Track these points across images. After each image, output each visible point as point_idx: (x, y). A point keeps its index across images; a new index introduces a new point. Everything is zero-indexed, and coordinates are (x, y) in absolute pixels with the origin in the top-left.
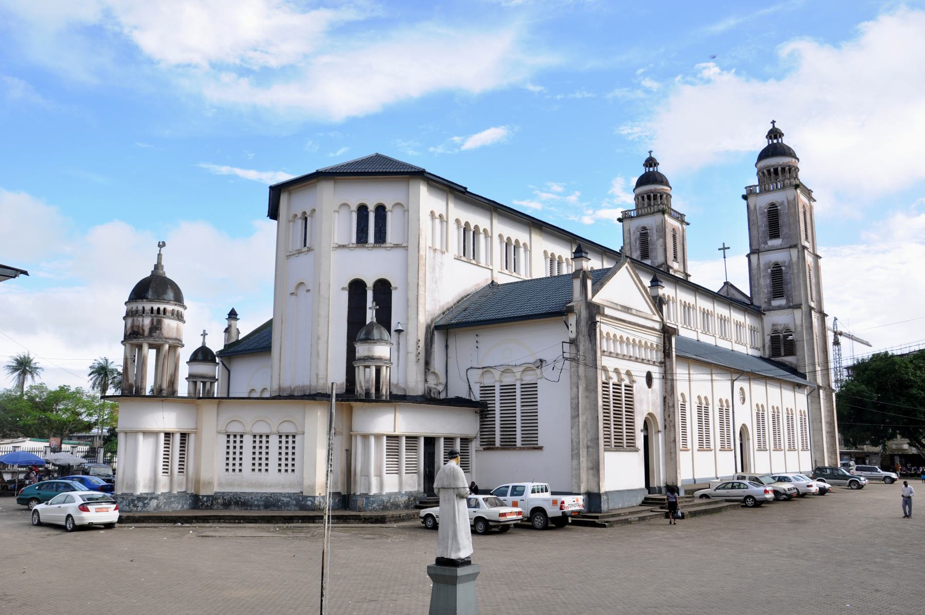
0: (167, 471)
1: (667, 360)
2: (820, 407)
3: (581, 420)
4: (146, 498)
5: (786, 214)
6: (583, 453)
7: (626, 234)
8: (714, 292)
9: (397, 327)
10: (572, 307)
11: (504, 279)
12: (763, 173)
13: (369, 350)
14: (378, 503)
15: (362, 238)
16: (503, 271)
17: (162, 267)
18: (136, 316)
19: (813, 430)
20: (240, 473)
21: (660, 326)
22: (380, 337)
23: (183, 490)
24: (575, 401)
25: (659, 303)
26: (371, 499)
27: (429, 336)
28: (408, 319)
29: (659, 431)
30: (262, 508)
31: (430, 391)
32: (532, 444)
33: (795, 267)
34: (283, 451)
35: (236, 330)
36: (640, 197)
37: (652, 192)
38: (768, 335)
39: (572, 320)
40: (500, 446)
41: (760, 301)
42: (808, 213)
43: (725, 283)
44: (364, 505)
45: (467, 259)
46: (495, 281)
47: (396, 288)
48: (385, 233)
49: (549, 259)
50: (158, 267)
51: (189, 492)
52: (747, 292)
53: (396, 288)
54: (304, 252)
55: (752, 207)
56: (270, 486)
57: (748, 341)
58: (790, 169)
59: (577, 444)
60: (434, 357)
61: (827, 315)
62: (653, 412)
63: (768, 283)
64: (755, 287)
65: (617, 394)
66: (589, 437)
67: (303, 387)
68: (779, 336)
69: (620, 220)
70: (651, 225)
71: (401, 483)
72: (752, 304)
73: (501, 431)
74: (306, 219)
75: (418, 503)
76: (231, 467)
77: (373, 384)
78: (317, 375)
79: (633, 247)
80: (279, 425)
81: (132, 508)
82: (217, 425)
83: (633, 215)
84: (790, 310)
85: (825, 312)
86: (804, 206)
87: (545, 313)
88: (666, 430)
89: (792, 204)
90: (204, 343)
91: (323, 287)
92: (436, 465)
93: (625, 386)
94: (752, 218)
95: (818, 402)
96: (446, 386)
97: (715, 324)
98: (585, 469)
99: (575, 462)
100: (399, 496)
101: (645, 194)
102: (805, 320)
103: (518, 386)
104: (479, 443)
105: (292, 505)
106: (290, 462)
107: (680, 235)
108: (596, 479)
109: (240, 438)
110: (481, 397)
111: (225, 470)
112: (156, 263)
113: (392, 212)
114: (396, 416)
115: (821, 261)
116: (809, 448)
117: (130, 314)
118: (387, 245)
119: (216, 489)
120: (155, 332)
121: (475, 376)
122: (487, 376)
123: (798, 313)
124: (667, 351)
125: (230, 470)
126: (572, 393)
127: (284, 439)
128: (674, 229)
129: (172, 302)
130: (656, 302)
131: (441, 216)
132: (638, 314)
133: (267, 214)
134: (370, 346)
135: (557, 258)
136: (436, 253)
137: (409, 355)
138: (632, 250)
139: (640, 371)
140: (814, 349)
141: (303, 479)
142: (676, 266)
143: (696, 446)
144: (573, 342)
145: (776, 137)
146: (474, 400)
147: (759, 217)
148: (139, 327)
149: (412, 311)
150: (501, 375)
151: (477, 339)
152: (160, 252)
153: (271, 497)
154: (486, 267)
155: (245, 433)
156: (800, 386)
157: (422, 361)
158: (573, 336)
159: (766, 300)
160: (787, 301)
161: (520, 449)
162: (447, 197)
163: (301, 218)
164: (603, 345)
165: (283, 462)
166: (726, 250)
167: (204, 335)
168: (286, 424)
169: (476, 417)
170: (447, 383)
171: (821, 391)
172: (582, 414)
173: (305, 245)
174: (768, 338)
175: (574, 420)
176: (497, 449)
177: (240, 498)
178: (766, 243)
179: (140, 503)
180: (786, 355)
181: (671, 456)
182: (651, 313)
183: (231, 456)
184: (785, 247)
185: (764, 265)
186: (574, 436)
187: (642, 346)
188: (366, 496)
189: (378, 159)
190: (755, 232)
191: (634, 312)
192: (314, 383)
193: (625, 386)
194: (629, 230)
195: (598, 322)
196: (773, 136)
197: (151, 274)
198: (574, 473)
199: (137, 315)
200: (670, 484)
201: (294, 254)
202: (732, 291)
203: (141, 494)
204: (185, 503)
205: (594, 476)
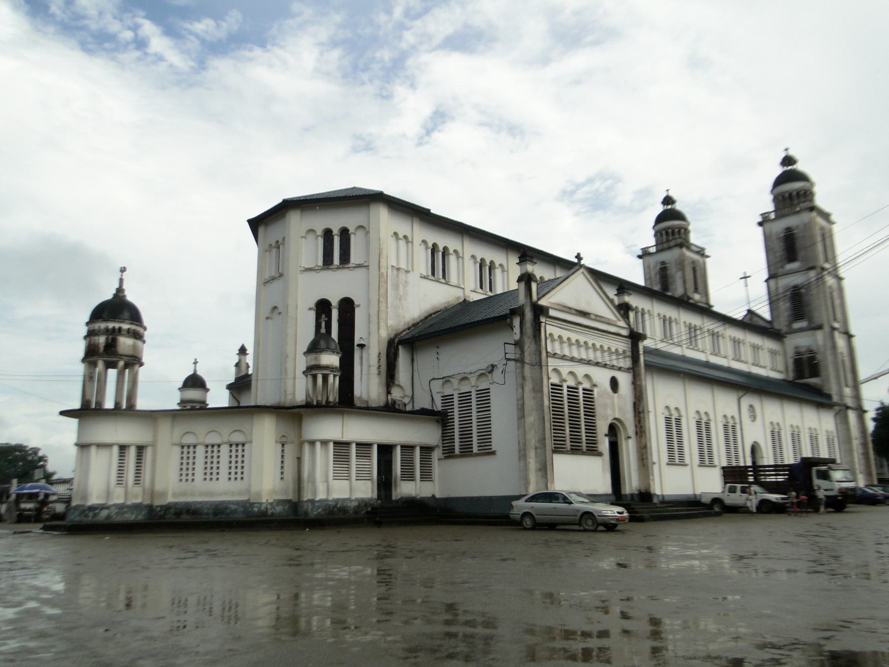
13: (316, 359)
16: (476, 290)
24: (521, 402)
25: (624, 309)
29: (629, 437)
32: (487, 451)
40: (459, 453)
41: (781, 325)
47: (359, 306)
50: (120, 290)
53: (359, 306)
62: (620, 418)
76: (184, 478)
78: (285, 391)
80: (231, 433)
93: (584, 389)
96: (412, 398)
99: (522, 463)
101: (663, 230)
104: (442, 451)
106: (239, 470)
110: (443, 406)
113: (355, 234)
117: (91, 334)
118: (350, 265)
119: (170, 499)
122: (448, 385)
123: (819, 335)
129: (128, 321)
136: (400, 272)
137: (371, 368)
139: (602, 377)
143: (696, 460)
144: (518, 344)
146: (436, 410)
149: (374, 326)
161: (477, 455)
162: (412, 220)
167: (195, 363)
170: (413, 395)
174: (790, 362)
180: (811, 377)
188: (312, 501)
191: (593, 317)
192: (283, 400)
195: (542, 322)
200: (643, 491)
201: (269, 281)
202: (756, 319)
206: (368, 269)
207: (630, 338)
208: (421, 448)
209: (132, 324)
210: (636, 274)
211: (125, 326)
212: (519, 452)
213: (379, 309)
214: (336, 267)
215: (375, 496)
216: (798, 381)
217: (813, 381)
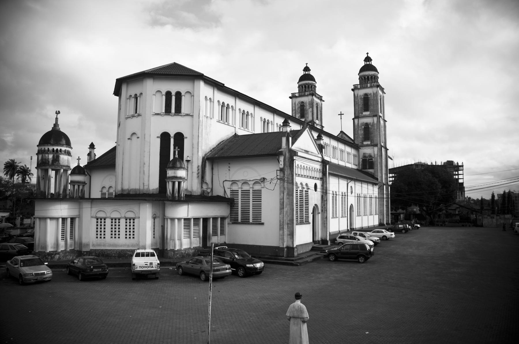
0: (63, 238)
1: (324, 177)
3: (285, 210)
4: (53, 254)
5: (372, 99)
6: (286, 227)
7: (293, 105)
8: (335, 136)
9: (187, 158)
10: (282, 152)
11: (241, 132)
13: (175, 173)
14: (179, 254)
15: (168, 111)
16: (240, 128)
17: (58, 125)
18: (44, 153)
19: (380, 205)
20: (104, 239)
21: (321, 159)
22: (181, 166)
23: (73, 248)
25: (321, 148)
26: (176, 252)
27: (204, 163)
28: (193, 154)
29: (319, 213)
30: (117, 258)
31: (204, 192)
33: (375, 126)
34: (128, 227)
35: (94, 154)
36: (301, 87)
37: (307, 84)
38: (361, 158)
39: (282, 159)
42: (382, 99)
43: (341, 131)
44: (172, 256)
45: (223, 121)
46: (237, 133)
47: (186, 138)
49: (263, 122)
50: (56, 125)
51: (76, 249)
52: (352, 138)
53: (186, 138)
54: (136, 116)
55: (356, 95)
56: (121, 246)
57: (352, 162)
58: (375, 77)
60: (206, 175)
61: (388, 150)
63: (362, 133)
64: (356, 135)
65: (301, 196)
66: (289, 219)
67: (135, 189)
68: (366, 159)
69: (290, 98)
70: (306, 101)
71: (191, 243)
72: (354, 143)
73: (253, 218)
74: (136, 98)
75: (199, 253)
77: (176, 191)
78: (144, 183)
79: (297, 112)
81: (45, 260)
82: (91, 213)
83: (297, 95)
84: (372, 147)
85: (387, 148)
86: (380, 96)
87: (267, 154)
88: (323, 212)
89: (375, 95)
90: (79, 164)
92: (208, 232)
97: (338, 153)
98: (286, 235)
99: (281, 232)
100: (190, 250)
101: (304, 85)
102: (379, 152)
103: (251, 191)
107: (320, 107)
110: (231, 196)
111: (96, 237)
112: (55, 123)
113: (184, 96)
115: (386, 123)
116: (378, 213)
117: (39, 153)
119: (91, 248)
120: (55, 163)
123: (376, 149)
125: (99, 238)
126: (281, 196)
128: (317, 104)
129: (65, 146)
130: (320, 148)
131: (210, 99)
132: (312, 154)
134: (175, 171)
135: (267, 121)
136: (208, 119)
137: (194, 173)
138: (296, 113)
139: (311, 183)
140: (382, 166)
141: (139, 242)
142: (317, 122)
144: (282, 170)
145: (368, 61)
146: (227, 197)
147: (359, 100)
148: (46, 159)
149: (195, 150)
150: (242, 185)
153: (122, 252)
154: (233, 126)
155: (107, 218)
156: (376, 184)
157: (200, 177)
158: (282, 166)
159: (361, 141)
160: (371, 142)
161: (252, 224)
163: (134, 97)
164: (297, 171)
166: (342, 115)
168: (129, 213)
169: (228, 206)
170: (212, 188)
171: (385, 186)
172: (285, 207)
173: (136, 113)
174: (361, 160)
175: (281, 210)
177: (105, 252)
179: (49, 257)
180: (369, 169)
181: (324, 225)
182: (318, 153)
183: (99, 230)
185: (361, 124)
186: (281, 219)
187: (313, 170)
188: (173, 251)
189: (175, 66)
190: (357, 108)
191: (310, 153)
192: (142, 188)
193: (305, 191)
194: (295, 103)
196: (367, 60)
198: (281, 237)
199: (45, 153)
200: (323, 239)
201: (130, 117)
204: (74, 256)
205: (291, 238)
206: (193, 117)
207: (322, 163)
208: (221, 218)
209: (67, 147)
210: (287, 108)
211: (63, 149)
213: (198, 141)
214: (174, 114)
215: (201, 246)
216: (363, 170)
217: (371, 171)
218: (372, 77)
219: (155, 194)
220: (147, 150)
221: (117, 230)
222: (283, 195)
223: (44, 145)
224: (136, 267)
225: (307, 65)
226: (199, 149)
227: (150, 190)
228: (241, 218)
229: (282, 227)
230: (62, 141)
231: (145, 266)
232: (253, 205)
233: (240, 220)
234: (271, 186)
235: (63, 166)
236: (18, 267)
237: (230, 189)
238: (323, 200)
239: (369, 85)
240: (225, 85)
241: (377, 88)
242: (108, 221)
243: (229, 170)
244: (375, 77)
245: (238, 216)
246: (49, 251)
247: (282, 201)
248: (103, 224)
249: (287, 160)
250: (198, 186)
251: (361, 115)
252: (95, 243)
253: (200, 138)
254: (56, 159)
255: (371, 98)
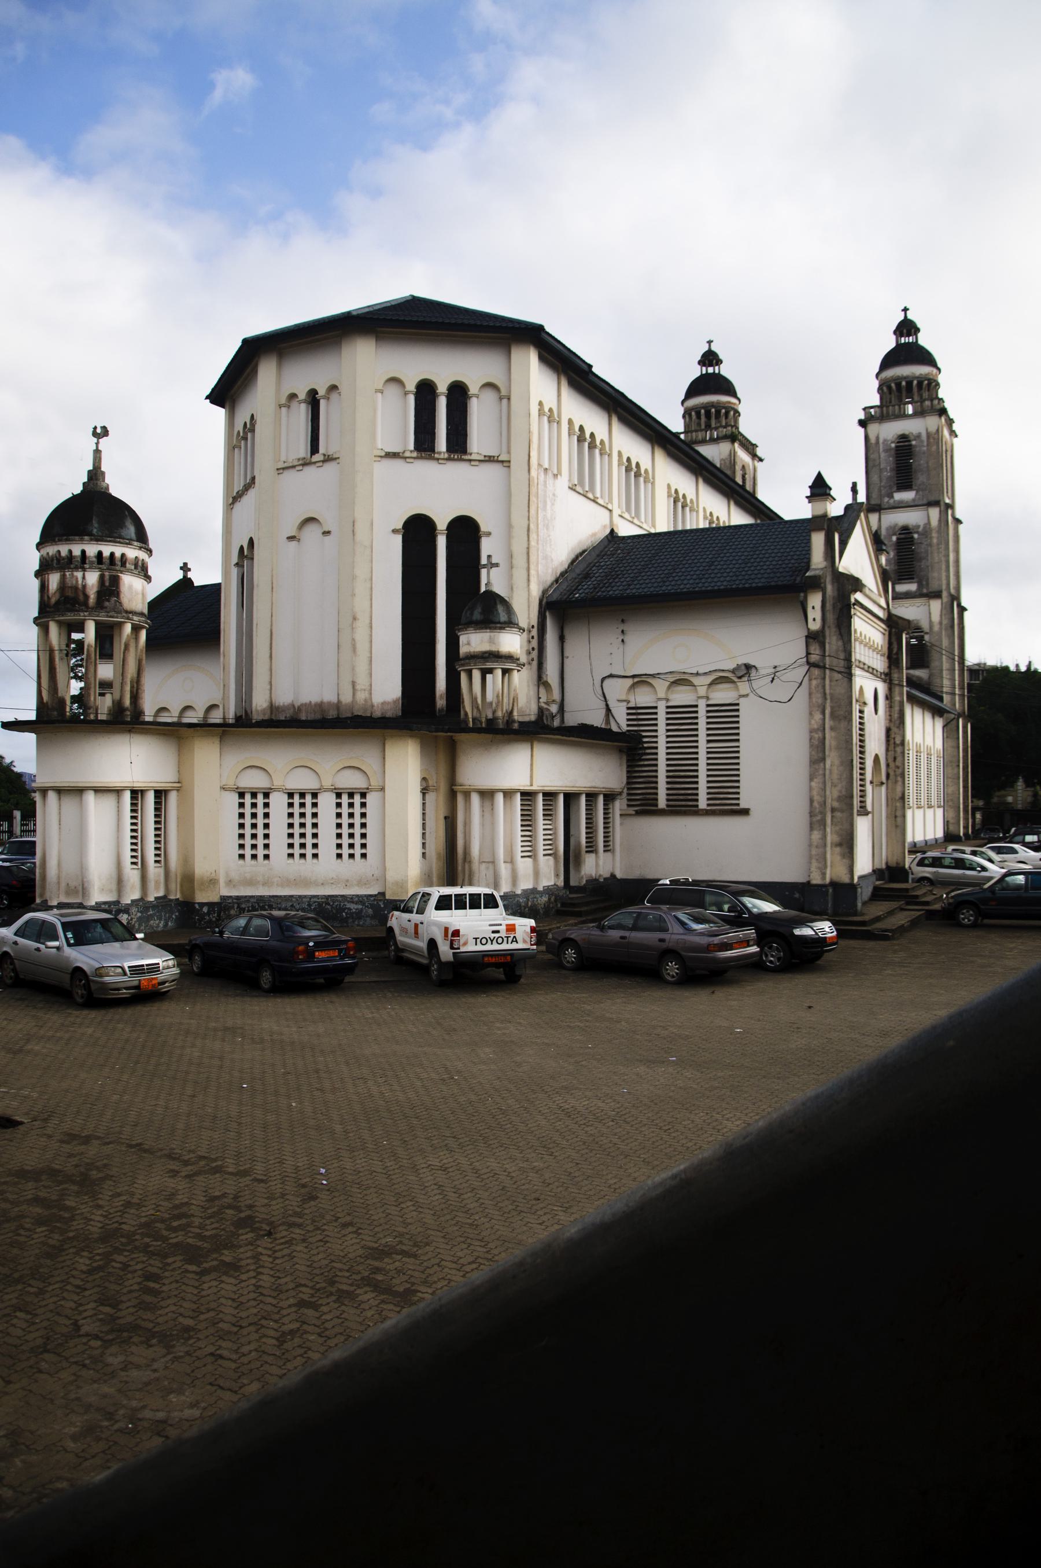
2: (959, 744)
5: (924, 453)
11: (625, 530)
12: (889, 388)
13: (491, 641)
15: (424, 444)
18: (69, 568)
23: (161, 894)
28: (512, 589)
29: (882, 783)
33: (934, 535)
34: (345, 821)
36: (693, 413)
39: (815, 601)
46: (616, 530)
47: (489, 534)
48: (465, 435)
50: (95, 475)
51: (172, 897)
53: (489, 534)
54: (315, 463)
55: (873, 440)
58: (929, 385)
59: (821, 806)
67: (320, 705)
73: (708, 793)
75: (559, 905)
76: (248, 852)
78: (354, 683)
88: (889, 781)
89: (934, 439)
91: (361, 529)
94: (872, 456)
95: (955, 736)
99: (816, 835)
101: (703, 408)
105: (367, 917)
106: (358, 841)
108: (846, 861)
109: (349, 798)
110: (628, 725)
112: (91, 468)
114: (534, 758)
120: (108, 601)
121: (616, 690)
123: (936, 606)
124: (895, 657)
127: (345, 800)
128: (743, 467)
133: (208, 392)
134: (492, 634)
145: (909, 335)
146: (615, 728)
147: (883, 455)
148: (75, 588)
150: (669, 687)
151: (622, 627)
152: (97, 447)
155: (275, 790)
158: (815, 626)
161: (707, 813)
163: (305, 401)
165: (345, 841)
169: (621, 758)
173: (314, 448)
176: (662, 813)
178: (891, 496)
183: (248, 831)
184: (920, 503)
186: (815, 793)
189: (414, 304)
190: (875, 478)
192: (346, 698)
196: (905, 331)
197: (82, 489)
199: (72, 566)
201: (293, 467)
203: (96, 903)
204: (170, 917)
205: (843, 856)
206: (509, 467)
212: (812, 814)
218: (920, 384)
219: (389, 718)
220: (361, 572)
221: (309, 831)
222: (821, 716)
223: (68, 540)
224: (462, 942)
225: (710, 346)
226: (532, 572)
227: (373, 706)
228: (668, 795)
229: (819, 818)
230: (125, 526)
231: (494, 935)
232: (708, 753)
233: (662, 803)
234: (781, 690)
235: (131, 612)
236: (58, 948)
237: (625, 704)
238: (892, 742)
239: (910, 409)
240: (594, 370)
241: (940, 416)
242: (278, 803)
243: (623, 641)
244: (929, 385)
245: (657, 788)
246: (96, 903)
247: (816, 736)
248: (260, 811)
249: (829, 606)
250: (529, 690)
251: (888, 502)
252: (234, 875)
253: (533, 536)
254: (110, 589)
255: (921, 447)
